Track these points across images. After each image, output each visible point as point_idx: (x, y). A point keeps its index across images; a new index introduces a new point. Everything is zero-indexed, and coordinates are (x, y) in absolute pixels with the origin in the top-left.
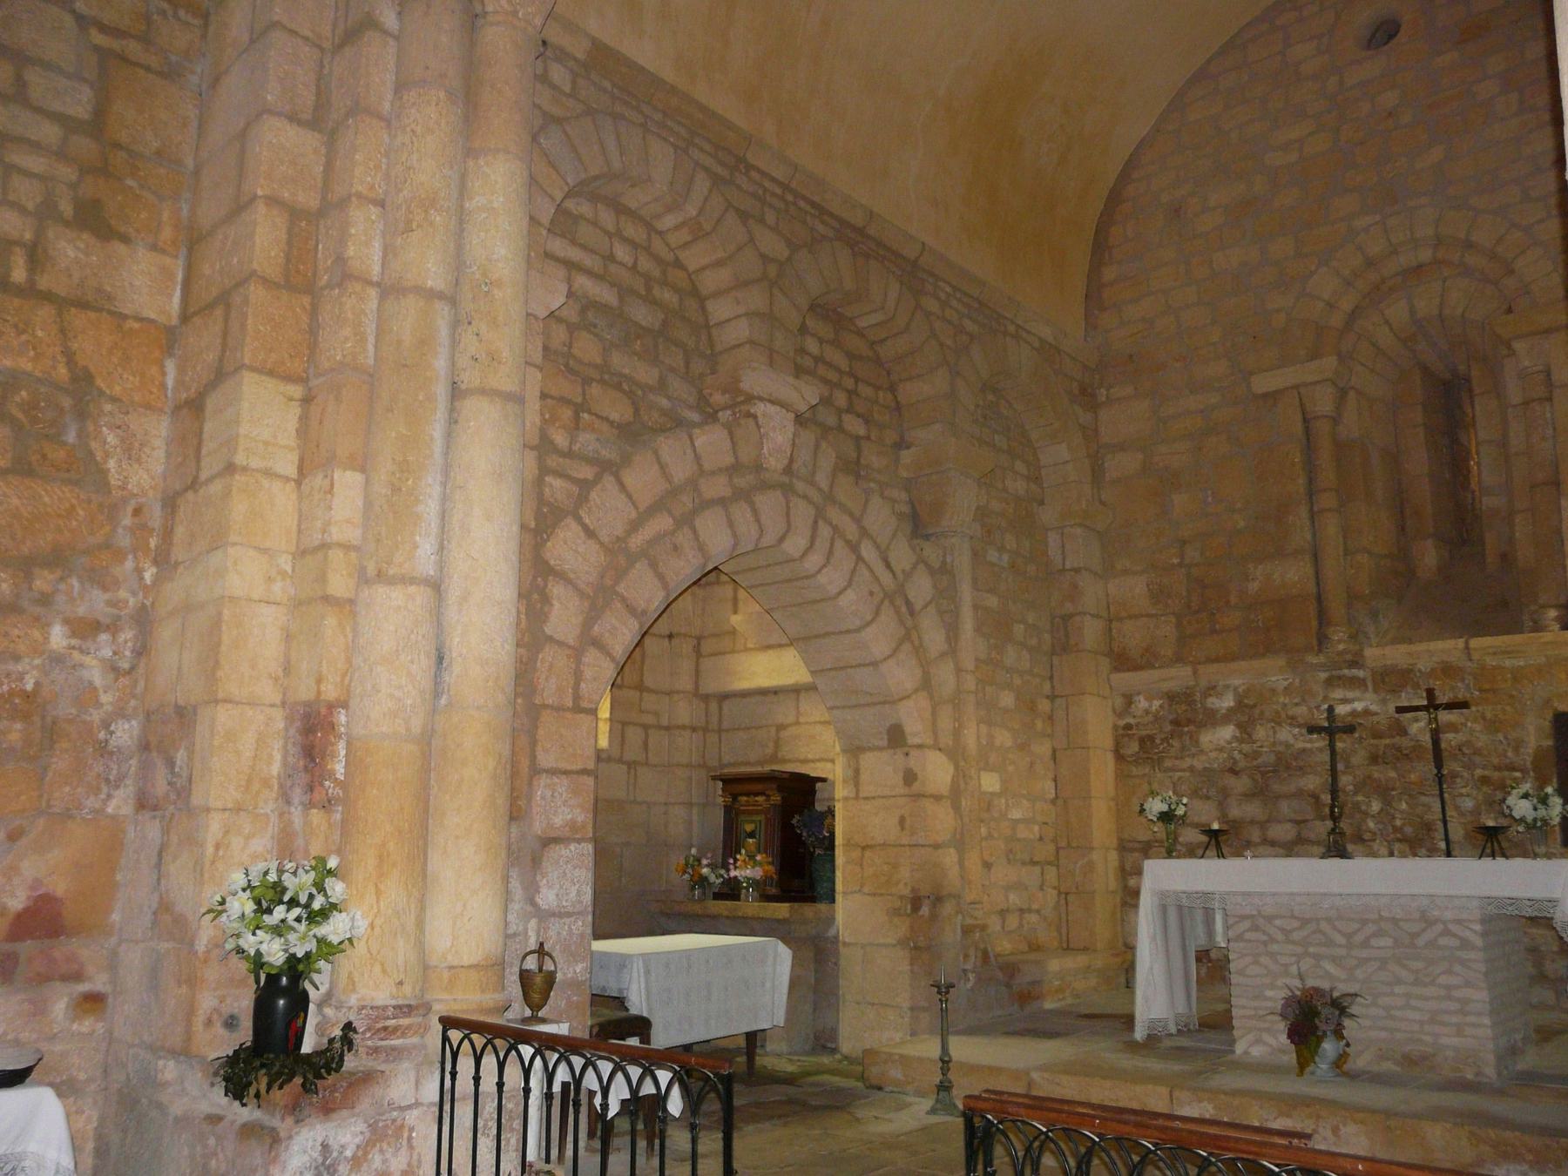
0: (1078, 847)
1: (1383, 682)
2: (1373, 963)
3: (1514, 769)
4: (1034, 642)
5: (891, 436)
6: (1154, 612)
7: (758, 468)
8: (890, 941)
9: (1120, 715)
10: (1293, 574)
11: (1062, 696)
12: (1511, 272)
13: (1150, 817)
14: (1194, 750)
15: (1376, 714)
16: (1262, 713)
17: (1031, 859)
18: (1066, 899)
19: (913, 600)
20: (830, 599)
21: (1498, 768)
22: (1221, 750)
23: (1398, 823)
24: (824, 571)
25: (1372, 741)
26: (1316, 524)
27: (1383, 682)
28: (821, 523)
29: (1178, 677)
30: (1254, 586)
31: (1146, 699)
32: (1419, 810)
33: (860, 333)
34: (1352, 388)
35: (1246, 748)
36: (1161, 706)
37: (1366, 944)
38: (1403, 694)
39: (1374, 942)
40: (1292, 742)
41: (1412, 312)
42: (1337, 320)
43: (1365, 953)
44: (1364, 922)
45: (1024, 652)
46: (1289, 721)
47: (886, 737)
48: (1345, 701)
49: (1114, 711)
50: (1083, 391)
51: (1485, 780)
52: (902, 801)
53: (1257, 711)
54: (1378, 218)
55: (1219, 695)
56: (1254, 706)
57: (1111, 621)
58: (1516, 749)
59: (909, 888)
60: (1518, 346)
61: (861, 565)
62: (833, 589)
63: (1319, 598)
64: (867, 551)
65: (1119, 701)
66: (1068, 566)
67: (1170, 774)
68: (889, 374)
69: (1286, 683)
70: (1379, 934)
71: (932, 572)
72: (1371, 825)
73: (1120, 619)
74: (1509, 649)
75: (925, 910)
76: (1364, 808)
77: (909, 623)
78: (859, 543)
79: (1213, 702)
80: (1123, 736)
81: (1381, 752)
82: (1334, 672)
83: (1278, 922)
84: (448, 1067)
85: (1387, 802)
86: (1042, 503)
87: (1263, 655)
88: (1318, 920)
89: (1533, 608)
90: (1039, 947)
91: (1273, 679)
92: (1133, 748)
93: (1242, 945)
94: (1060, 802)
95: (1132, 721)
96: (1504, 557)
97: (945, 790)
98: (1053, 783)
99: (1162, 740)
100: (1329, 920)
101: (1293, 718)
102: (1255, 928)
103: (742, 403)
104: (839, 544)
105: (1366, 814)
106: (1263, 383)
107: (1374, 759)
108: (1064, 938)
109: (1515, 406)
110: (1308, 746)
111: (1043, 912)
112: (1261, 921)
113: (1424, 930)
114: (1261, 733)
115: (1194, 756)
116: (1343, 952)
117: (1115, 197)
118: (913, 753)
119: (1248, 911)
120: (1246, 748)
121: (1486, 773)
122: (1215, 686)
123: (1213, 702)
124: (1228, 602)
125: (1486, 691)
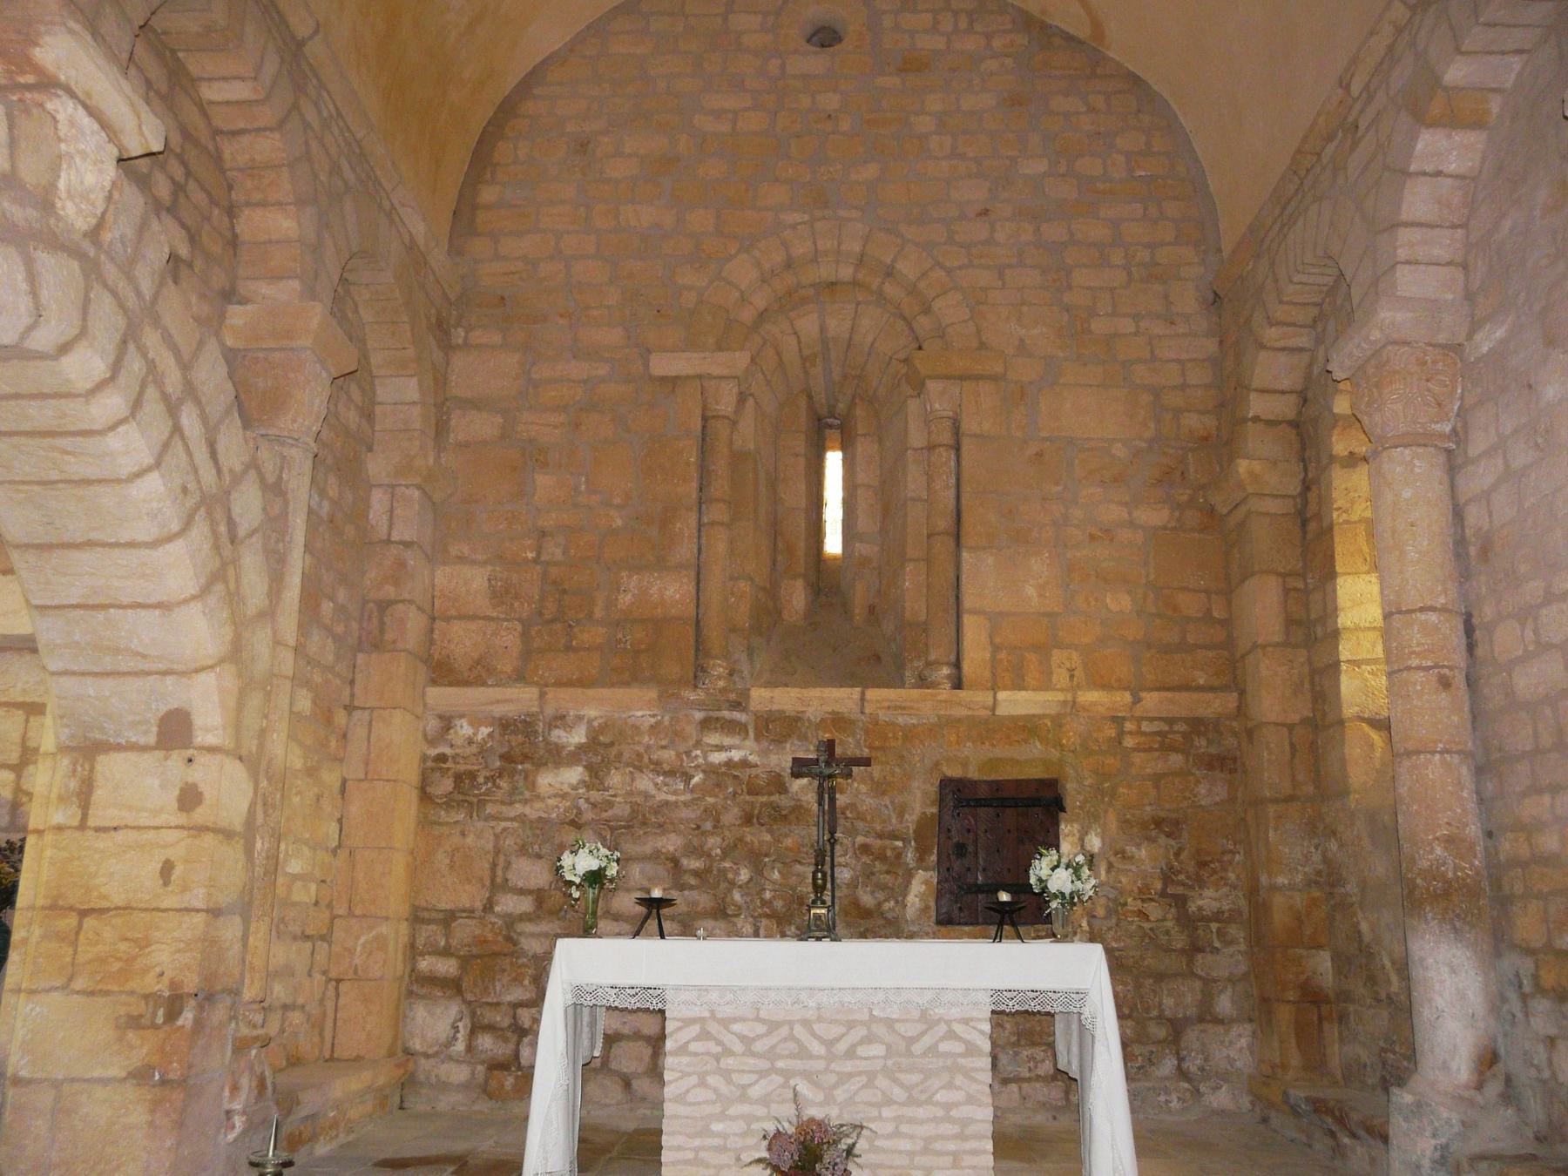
0: (364, 916)
1: (768, 730)
2: (858, 1079)
3: (897, 838)
4: (340, 629)
5: (219, 279)
6: (495, 614)
7: (46, 202)
8: (114, 1072)
9: (432, 742)
10: (673, 591)
11: (364, 709)
12: (927, 310)
13: (569, 877)
14: (527, 794)
15: (756, 766)
16: (620, 755)
17: (303, 932)
18: (337, 988)
19: (237, 519)
20: (119, 481)
21: (880, 836)
22: (564, 796)
23: (768, 895)
24: (121, 429)
25: (748, 798)
27: (768, 730)
28: (131, 347)
29: (519, 699)
30: (625, 600)
31: (471, 724)
32: (793, 880)
33: (203, 108)
34: (752, 395)
35: (595, 795)
36: (490, 735)
37: (850, 1054)
38: (788, 745)
39: (861, 1051)
40: (653, 792)
41: (823, 329)
42: (747, 315)
43: (848, 1066)
44: (851, 1025)
45: (330, 640)
46: (652, 767)
47: (155, 729)
48: (720, 748)
49: (425, 736)
50: (440, 323)
51: (865, 849)
52: (169, 836)
53: (614, 751)
54: (806, 217)
55: (569, 728)
56: (612, 744)
57: (433, 619)
58: (901, 815)
59: (166, 980)
60: (933, 386)
61: (176, 438)
62: (127, 466)
63: (698, 622)
64: (189, 420)
65: (433, 724)
66: (395, 537)
67: (493, 823)
68: (230, 187)
69: (653, 720)
70: (869, 1039)
71: (264, 486)
72: (737, 896)
73: (448, 619)
74: (903, 705)
75: (187, 1018)
76: (730, 876)
77: (227, 551)
78: (181, 401)
79: (559, 735)
80: (433, 769)
81: (756, 812)
82: (711, 713)
83: (736, 1027)
85: (758, 870)
86: (370, 449)
87: (627, 684)
88: (791, 1023)
89: (919, 664)
90: (298, 1059)
91: (639, 714)
92: (445, 786)
93: (685, 1060)
94: (342, 854)
95: (448, 751)
96: (872, 609)
97: (238, 823)
98: (338, 826)
99: (486, 778)
100: (806, 1023)
101: (657, 763)
102: (705, 1035)
103: (28, 87)
104: (152, 393)
105: (732, 884)
106: (663, 365)
107: (748, 819)
108: (328, 1045)
109: (915, 450)
110: (672, 798)
111: (307, 1008)
112: (713, 1028)
113: (923, 1033)
114: (615, 779)
115: (526, 802)
116: (821, 1065)
117: (507, 109)
118: (203, 759)
119: (695, 1012)
120: (595, 795)
121: (868, 841)
122: (564, 716)
123: (559, 735)
124: (590, 616)
125: (877, 749)
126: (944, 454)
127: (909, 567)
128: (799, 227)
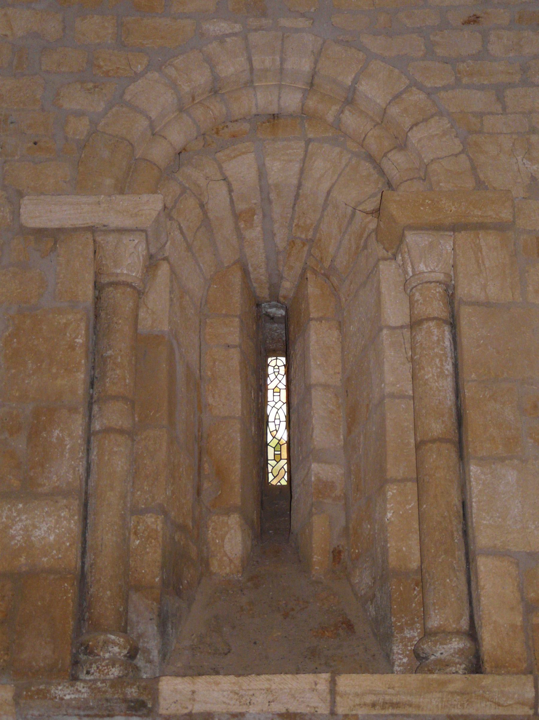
26: (94, 452)
34: (165, 259)
41: (262, 174)
54: (238, 27)
84: (287, 338)
109: (393, 328)
126: (436, 331)
127: (391, 491)
128: (228, 40)
